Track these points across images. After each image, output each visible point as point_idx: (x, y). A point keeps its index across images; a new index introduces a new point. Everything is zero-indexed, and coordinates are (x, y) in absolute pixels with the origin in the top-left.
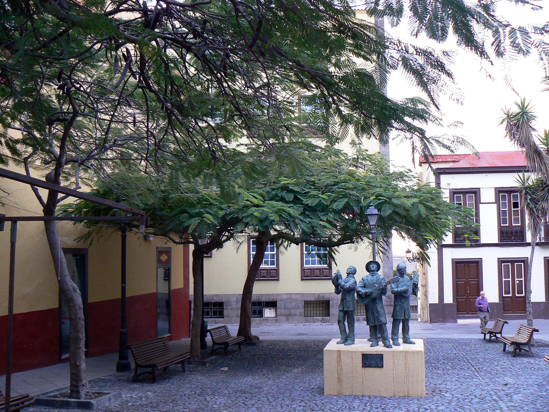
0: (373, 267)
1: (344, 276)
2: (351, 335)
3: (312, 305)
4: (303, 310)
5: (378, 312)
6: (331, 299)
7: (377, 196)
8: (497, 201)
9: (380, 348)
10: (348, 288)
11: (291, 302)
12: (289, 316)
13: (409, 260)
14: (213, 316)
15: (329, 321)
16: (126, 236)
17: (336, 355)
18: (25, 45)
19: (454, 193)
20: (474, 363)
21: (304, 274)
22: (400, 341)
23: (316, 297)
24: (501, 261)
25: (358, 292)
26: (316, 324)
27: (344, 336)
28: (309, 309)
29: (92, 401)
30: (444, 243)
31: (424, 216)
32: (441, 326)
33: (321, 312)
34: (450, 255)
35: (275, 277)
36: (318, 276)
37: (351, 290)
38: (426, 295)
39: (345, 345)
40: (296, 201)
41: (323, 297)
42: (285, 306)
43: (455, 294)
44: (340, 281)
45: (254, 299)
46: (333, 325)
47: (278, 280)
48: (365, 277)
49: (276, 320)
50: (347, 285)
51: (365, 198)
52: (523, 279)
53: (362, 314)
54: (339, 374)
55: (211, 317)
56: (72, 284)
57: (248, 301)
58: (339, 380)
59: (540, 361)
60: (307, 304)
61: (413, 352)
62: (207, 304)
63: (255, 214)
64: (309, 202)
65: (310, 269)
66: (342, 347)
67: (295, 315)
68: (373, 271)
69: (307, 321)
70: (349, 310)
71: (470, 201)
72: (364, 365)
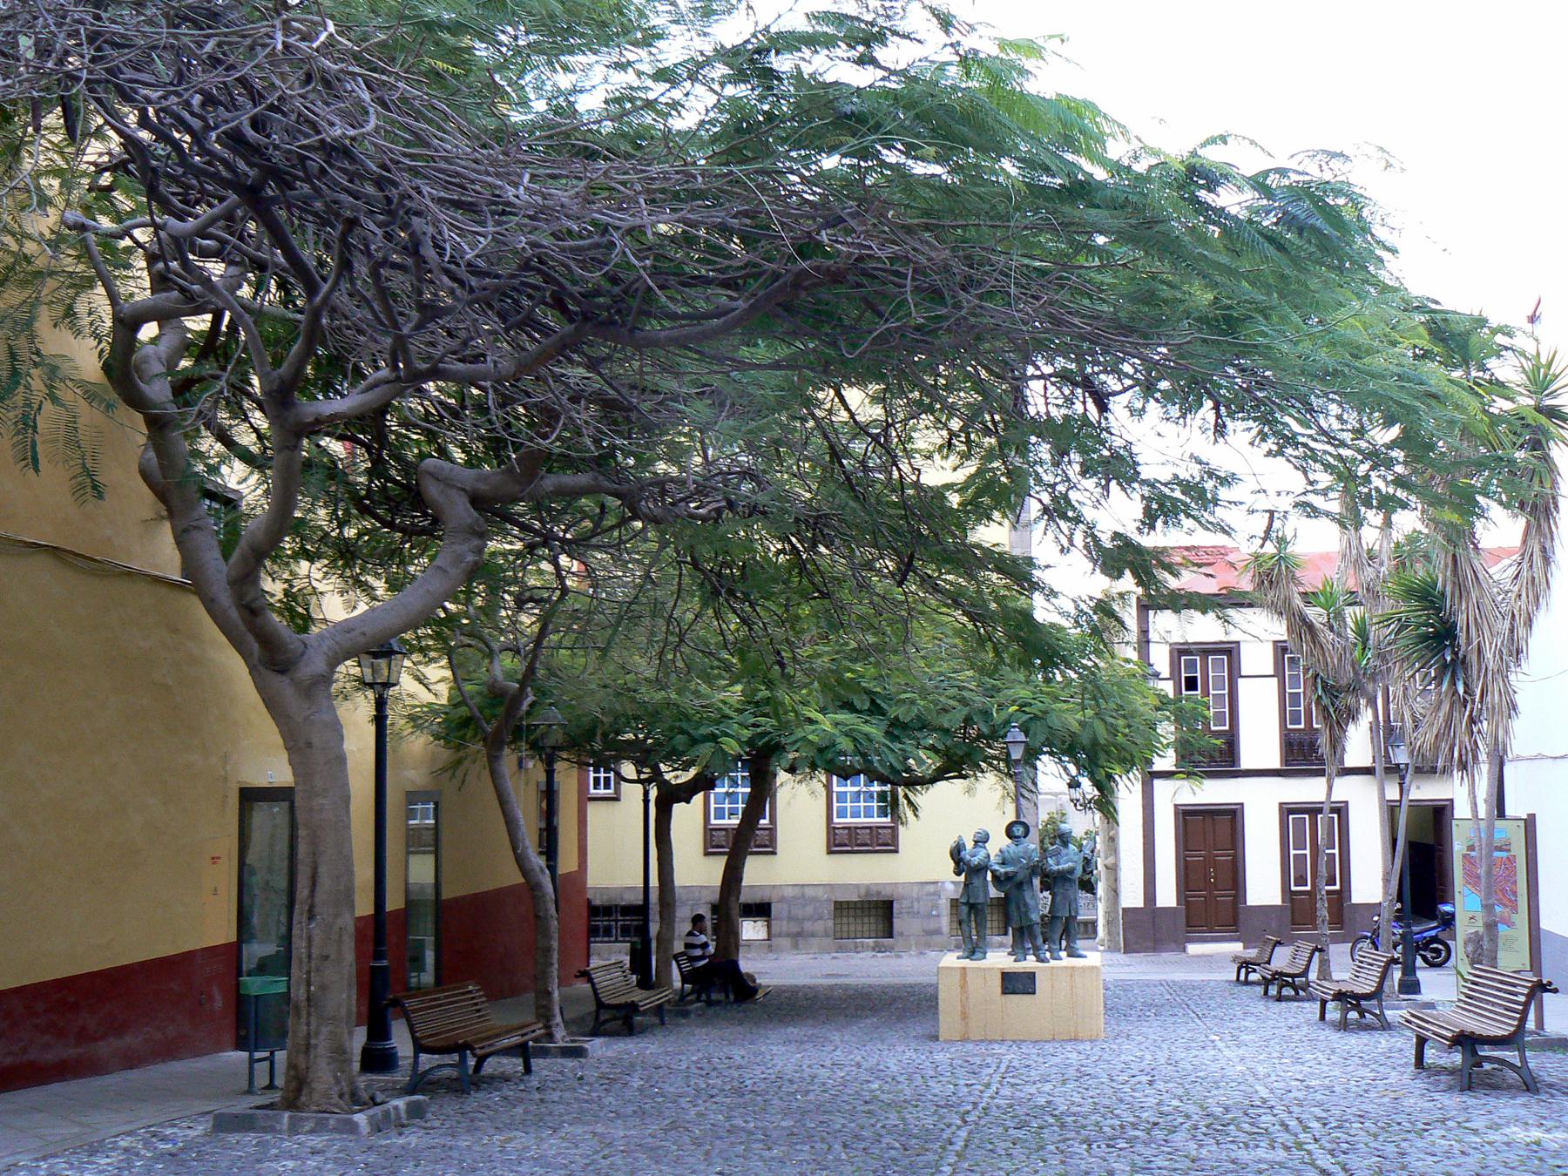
0: (1019, 830)
1: (969, 845)
2: (981, 945)
3: (852, 912)
4: (831, 923)
5: (1026, 905)
6: (895, 896)
7: (1021, 706)
8: (1279, 672)
9: (1030, 963)
11: (805, 905)
12: (799, 938)
15: (891, 949)
17: (958, 975)
19: (1180, 652)
23: (863, 892)
24: (1287, 810)
25: (993, 872)
26: (861, 955)
29: (586, 1046)
30: (1156, 768)
31: (1103, 742)
32: (1153, 958)
33: (873, 927)
34: (1172, 795)
36: (867, 845)
37: (981, 869)
38: (1114, 892)
40: (875, 710)
41: (879, 893)
45: (745, 897)
46: (899, 957)
47: (774, 853)
48: (1004, 847)
50: (975, 860)
54: (963, 1006)
55: (616, 941)
56: (539, 862)
57: (733, 899)
58: (965, 1016)
60: (841, 908)
61: (1084, 969)
62: (594, 911)
63: (810, 737)
65: (849, 828)
66: (967, 963)
67: (813, 935)
69: (840, 949)
71: (1216, 670)
72: (1005, 991)
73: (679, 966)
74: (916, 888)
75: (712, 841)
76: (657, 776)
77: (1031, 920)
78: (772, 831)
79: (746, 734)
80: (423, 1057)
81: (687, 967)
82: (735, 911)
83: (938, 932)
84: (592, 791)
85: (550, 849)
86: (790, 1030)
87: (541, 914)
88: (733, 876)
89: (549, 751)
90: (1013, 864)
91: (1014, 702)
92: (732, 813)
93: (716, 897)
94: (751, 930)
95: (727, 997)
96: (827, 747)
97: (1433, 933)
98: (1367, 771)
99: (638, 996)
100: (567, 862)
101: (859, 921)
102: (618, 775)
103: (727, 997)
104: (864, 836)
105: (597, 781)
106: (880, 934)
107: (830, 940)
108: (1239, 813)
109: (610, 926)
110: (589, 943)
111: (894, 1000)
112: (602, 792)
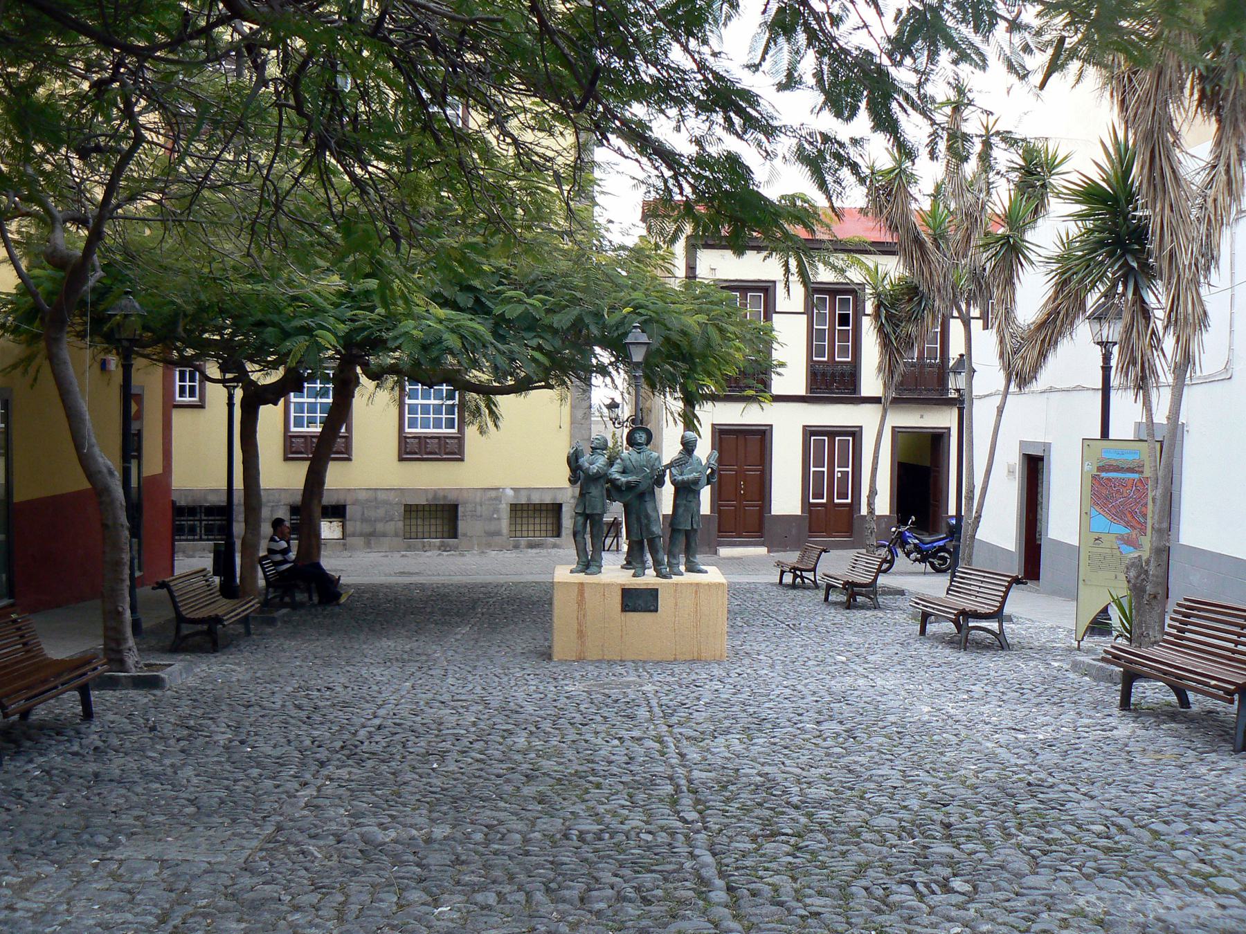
4: (401, 524)
5: (648, 517)
7: (635, 308)
8: (808, 310)
9: (649, 578)
10: (595, 474)
11: (377, 508)
12: (371, 537)
13: (614, 423)
14: (204, 537)
15: (455, 548)
16: (131, 365)
20: (780, 618)
21: (406, 447)
22: (682, 568)
23: (430, 496)
24: (810, 432)
26: (428, 554)
27: (584, 559)
28: (413, 522)
33: (440, 529)
35: (342, 453)
39: (587, 574)
40: (479, 308)
41: (445, 497)
42: (363, 514)
43: (716, 496)
44: (581, 460)
45: (327, 500)
46: (463, 555)
47: (349, 459)
49: (344, 545)
51: (612, 309)
52: (850, 469)
53: (525, 534)
54: (580, 624)
55: (201, 539)
57: (316, 502)
58: (581, 634)
59: (894, 615)
60: (411, 511)
62: (179, 511)
64: (512, 311)
65: (419, 438)
66: (581, 577)
67: (384, 535)
68: (640, 444)
69: (409, 548)
70: (595, 512)
71: (753, 308)
72: (625, 608)
73: (263, 569)
74: (479, 494)
75: (291, 447)
76: (243, 377)
77: (653, 533)
78: (348, 439)
79: (343, 328)
80: (183, 625)
81: (271, 570)
82: (317, 511)
83: (498, 533)
84: (178, 398)
85: (131, 446)
86: (385, 643)
87: (110, 523)
88: (315, 479)
89: (125, 344)
90: (637, 474)
91: (627, 304)
92: (311, 421)
93: (298, 499)
94: (329, 530)
95: (311, 598)
96: (431, 344)
97: (941, 543)
98: (875, 400)
99: (222, 607)
100: (152, 465)
101: (427, 523)
102: (203, 374)
103: (311, 598)
104: (433, 445)
105: (182, 389)
106: (446, 535)
107: (400, 539)
108: (768, 434)
109: (194, 525)
110: (173, 541)
111: (474, 603)
112: (187, 399)
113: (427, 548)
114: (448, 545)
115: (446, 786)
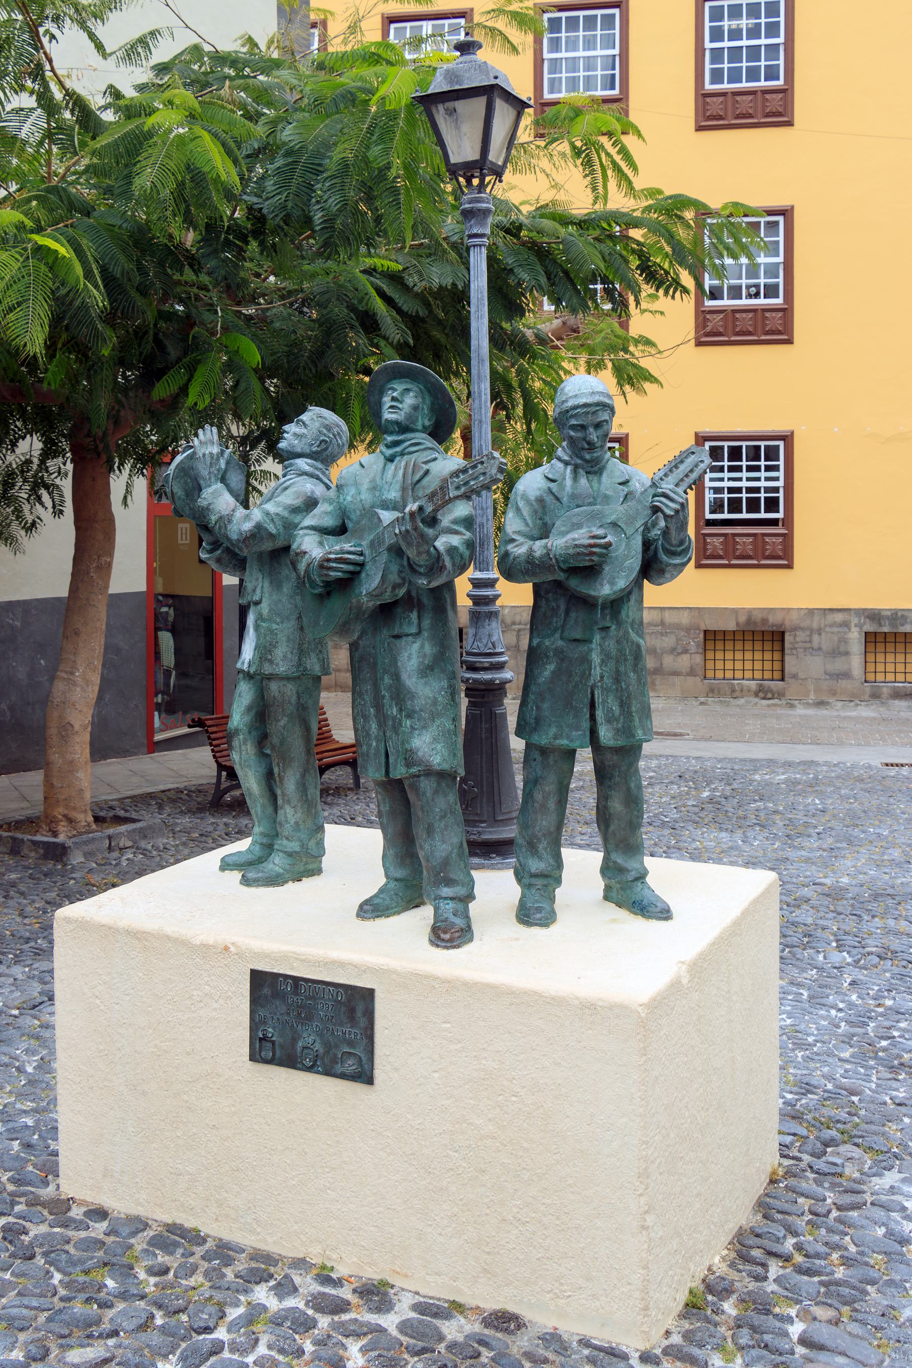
15: (780, 695)
18: (122, 439)
23: (742, 619)
26: (742, 701)
41: (765, 621)
67: (676, 673)
75: (705, 549)
83: (846, 675)
112: (781, 474)
113: (737, 694)
114: (771, 691)
115: (102, 814)
